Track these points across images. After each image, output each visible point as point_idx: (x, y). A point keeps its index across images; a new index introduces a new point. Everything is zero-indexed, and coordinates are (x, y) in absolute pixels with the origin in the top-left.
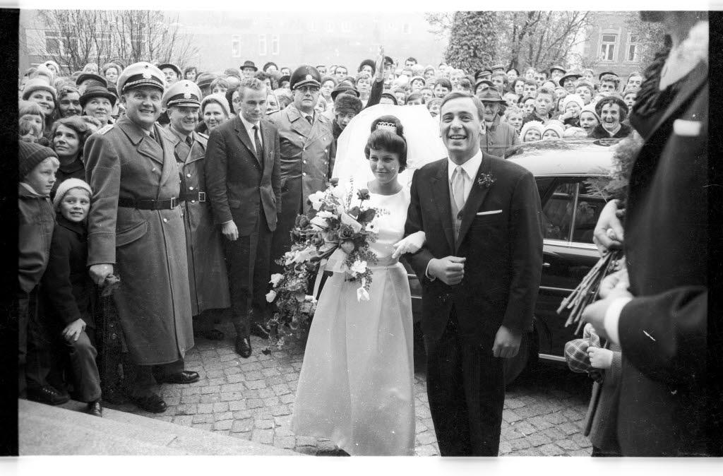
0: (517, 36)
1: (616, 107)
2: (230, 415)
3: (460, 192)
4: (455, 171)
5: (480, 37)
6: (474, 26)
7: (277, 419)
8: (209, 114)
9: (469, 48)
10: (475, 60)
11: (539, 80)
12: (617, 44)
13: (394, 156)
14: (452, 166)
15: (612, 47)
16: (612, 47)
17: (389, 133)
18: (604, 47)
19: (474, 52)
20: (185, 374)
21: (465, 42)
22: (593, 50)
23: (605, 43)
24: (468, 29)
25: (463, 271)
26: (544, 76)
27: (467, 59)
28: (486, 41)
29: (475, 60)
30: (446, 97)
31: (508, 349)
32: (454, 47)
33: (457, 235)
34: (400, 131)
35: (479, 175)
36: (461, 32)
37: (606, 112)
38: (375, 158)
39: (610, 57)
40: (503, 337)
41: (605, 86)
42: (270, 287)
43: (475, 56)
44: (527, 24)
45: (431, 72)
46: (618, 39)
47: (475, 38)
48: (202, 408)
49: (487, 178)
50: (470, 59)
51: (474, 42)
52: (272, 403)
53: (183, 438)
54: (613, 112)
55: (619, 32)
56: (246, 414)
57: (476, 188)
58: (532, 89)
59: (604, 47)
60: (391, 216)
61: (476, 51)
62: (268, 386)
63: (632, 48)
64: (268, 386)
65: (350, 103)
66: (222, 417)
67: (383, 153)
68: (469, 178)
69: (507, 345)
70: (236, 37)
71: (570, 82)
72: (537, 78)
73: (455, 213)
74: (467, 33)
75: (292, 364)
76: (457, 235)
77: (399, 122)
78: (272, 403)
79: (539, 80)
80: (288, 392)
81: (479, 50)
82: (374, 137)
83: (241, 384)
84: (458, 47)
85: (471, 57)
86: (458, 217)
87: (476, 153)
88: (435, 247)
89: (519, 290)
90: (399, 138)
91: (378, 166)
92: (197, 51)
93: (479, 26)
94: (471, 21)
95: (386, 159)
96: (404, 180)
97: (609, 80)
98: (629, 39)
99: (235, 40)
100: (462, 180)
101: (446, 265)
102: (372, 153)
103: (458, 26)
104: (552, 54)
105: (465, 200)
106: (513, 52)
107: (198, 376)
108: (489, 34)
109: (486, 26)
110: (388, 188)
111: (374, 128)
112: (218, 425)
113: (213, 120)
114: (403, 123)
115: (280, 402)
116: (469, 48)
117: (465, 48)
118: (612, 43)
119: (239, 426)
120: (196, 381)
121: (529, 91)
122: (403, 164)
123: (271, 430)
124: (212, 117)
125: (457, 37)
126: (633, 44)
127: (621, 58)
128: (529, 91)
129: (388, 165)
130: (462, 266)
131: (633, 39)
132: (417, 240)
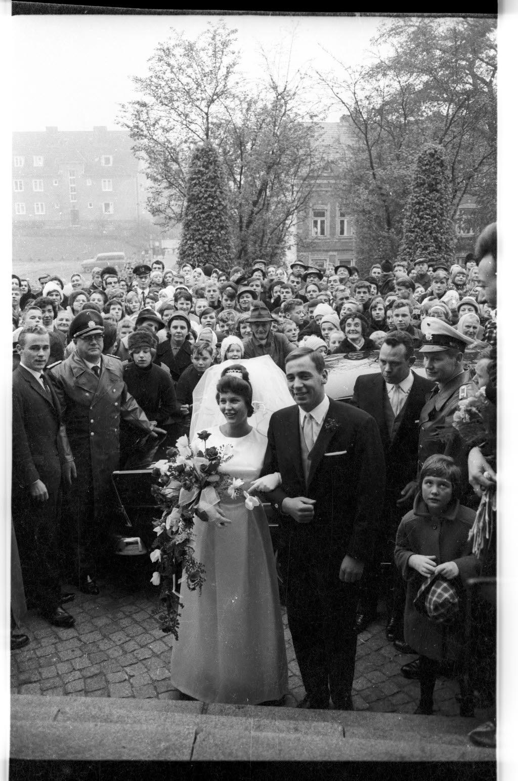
0: (244, 225)
2: (77, 674)
5: (214, 231)
6: (207, 221)
7: (128, 669)
9: (204, 243)
10: (210, 255)
11: (295, 284)
14: (302, 413)
15: (323, 222)
16: (323, 222)
18: (316, 222)
19: (209, 247)
23: (316, 219)
24: (201, 224)
26: (300, 280)
27: (202, 253)
28: (220, 235)
29: (210, 255)
33: (307, 474)
34: (246, 376)
35: (326, 421)
39: (322, 232)
40: (347, 564)
43: (210, 251)
45: (169, 275)
46: (328, 214)
47: (208, 232)
48: (46, 673)
50: (206, 255)
51: (209, 237)
52: (116, 653)
53: (67, 709)
55: (328, 207)
56: (94, 670)
58: (287, 292)
59: (316, 222)
60: (244, 456)
62: (105, 636)
63: (342, 222)
64: (105, 636)
65: (141, 338)
66: (71, 678)
71: (312, 279)
72: (293, 282)
73: (305, 456)
74: (201, 228)
75: (121, 609)
76: (307, 474)
77: (245, 369)
78: (116, 653)
79: (295, 284)
80: (128, 639)
83: (76, 639)
84: (192, 242)
85: (206, 251)
86: (308, 459)
88: (288, 488)
90: (245, 382)
93: (211, 221)
94: (203, 216)
98: (338, 214)
107: (27, 639)
108: (222, 228)
109: (218, 220)
110: (239, 429)
112: (69, 687)
115: (125, 652)
116: (204, 243)
117: (200, 242)
118: (323, 219)
119: (93, 684)
120: (27, 644)
123: (126, 682)
127: (333, 234)
128: (285, 294)
131: (342, 215)
132: (271, 481)
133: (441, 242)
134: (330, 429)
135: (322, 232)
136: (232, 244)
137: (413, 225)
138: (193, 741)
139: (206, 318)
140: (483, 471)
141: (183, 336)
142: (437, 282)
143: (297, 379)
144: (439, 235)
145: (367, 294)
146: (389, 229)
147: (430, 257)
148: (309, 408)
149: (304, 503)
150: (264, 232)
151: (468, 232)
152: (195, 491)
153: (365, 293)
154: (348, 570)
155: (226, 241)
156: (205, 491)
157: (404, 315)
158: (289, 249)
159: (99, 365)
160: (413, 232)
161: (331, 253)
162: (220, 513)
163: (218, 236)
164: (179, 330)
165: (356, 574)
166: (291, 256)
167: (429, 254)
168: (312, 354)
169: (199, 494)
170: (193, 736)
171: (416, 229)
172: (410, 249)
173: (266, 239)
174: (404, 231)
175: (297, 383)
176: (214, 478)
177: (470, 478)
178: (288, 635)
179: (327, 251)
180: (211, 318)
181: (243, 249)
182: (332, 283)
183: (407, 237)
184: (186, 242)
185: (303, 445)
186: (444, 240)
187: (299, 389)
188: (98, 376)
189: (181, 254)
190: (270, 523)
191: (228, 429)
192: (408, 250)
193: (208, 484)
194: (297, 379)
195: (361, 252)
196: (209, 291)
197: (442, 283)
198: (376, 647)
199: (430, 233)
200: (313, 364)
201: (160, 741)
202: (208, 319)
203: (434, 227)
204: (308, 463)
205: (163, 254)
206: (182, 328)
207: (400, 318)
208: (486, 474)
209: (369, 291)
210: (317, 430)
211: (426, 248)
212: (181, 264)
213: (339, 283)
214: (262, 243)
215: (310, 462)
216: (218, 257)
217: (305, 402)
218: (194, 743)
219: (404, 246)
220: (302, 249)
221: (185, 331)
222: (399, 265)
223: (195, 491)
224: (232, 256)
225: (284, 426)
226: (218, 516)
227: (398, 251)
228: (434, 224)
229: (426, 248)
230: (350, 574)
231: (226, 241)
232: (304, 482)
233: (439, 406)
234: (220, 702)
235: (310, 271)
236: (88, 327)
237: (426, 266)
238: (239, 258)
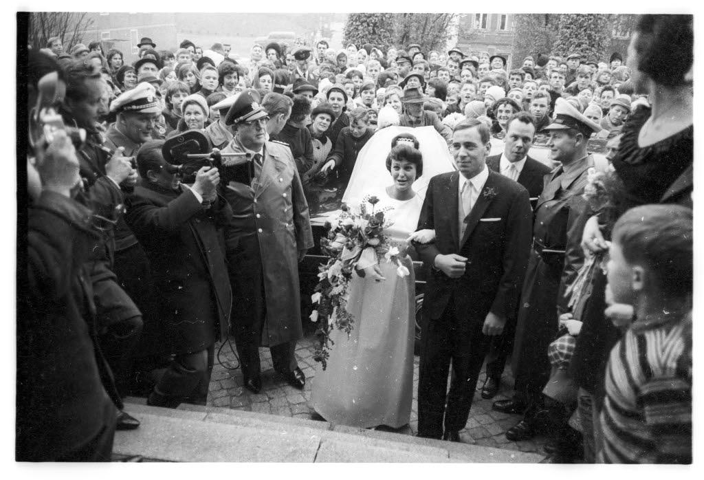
1: (509, 107)
3: (468, 199)
4: (465, 184)
8: (189, 113)
9: (368, 25)
11: (453, 68)
13: (413, 166)
14: (463, 180)
17: (409, 147)
19: (373, 29)
20: (237, 354)
21: (365, 19)
25: (465, 269)
30: (237, 65)
33: (462, 236)
34: (417, 146)
35: (484, 189)
37: (501, 111)
38: (397, 168)
39: (484, 26)
40: (490, 320)
41: (513, 79)
43: (374, 33)
49: (491, 191)
54: (507, 111)
57: (481, 199)
60: (404, 220)
61: (375, 29)
67: (404, 163)
68: (475, 190)
72: (451, 66)
73: (462, 218)
76: (462, 236)
81: (378, 27)
84: (358, 23)
85: (370, 34)
89: (506, 284)
91: (400, 174)
92: (93, 22)
95: (407, 168)
96: (420, 188)
97: (515, 74)
100: (469, 191)
101: (449, 261)
102: (394, 162)
104: (437, 27)
105: (472, 207)
106: (405, 26)
110: (404, 195)
111: (394, 144)
113: (193, 120)
114: (419, 140)
117: (365, 24)
121: (322, 49)
122: (419, 172)
124: (193, 117)
127: (493, 28)
129: (408, 173)
130: (464, 264)
133: (594, 40)
134: (488, 197)
135: (484, 26)
136: (394, 28)
137: (569, 22)
138: (317, 447)
139: (366, 93)
140: (594, 237)
141: (340, 107)
142: (581, 77)
143: (462, 148)
144: (593, 33)
145: (520, 82)
146: (546, 25)
147: (582, 54)
148: (469, 175)
149: (457, 260)
150: (427, 20)
151: (624, 35)
152: (357, 250)
153: (517, 80)
154: (492, 325)
155: (389, 24)
156: (366, 251)
157: (542, 106)
158: (450, 39)
159: (261, 152)
160: (569, 28)
161: (489, 47)
162: (376, 271)
163: (382, 19)
164: (336, 101)
165: (499, 329)
166: (451, 45)
167: (582, 51)
168: (480, 125)
169: (361, 252)
170: (318, 444)
171: (572, 26)
172: (564, 44)
173: (428, 27)
174: (560, 26)
175: (462, 151)
176: (375, 242)
177: (582, 244)
178: (416, 370)
179: (488, 45)
180: (371, 93)
181: (405, 34)
182: (482, 71)
183: (563, 33)
184: (352, 24)
185: (460, 209)
186: (597, 39)
187: (463, 158)
188: (261, 165)
189: (346, 35)
190: (417, 279)
191: (394, 191)
192: (562, 46)
193: (368, 246)
194: (462, 148)
195: (519, 46)
196: (371, 71)
197: (587, 77)
198: (149, 91)
199: (585, 30)
200: (479, 136)
201: (289, 445)
202: (369, 94)
203: (590, 25)
204: (463, 226)
205: (330, 37)
206: (339, 99)
207: (538, 108)
208: (595, 240)
209: (523, 79)
210: (476, 196)
211: (579, 45)
212: (346, 45)
213: (488, 70)
214: (424, 30)
215: (466, 225)
216: (381, 39)
217: (466, 169)
218: (318, 450)
219: (559, 42)
220: (463, 40)
221: (342, 103)
222: (553, 59)
223: (357, 250)
224: (394, 40)
225: (443, 190)
226: (375, 273)
227: (553, 46)
228: (590, 22)
229: (579, 45)
230: (493, 329)
231: (389, 24)
232: (458, 243)
233: (565, 185)
234: (346, 424)
235: (466, 59)
236: (252, 110)
237: (578, 62)
238: (401, 43)
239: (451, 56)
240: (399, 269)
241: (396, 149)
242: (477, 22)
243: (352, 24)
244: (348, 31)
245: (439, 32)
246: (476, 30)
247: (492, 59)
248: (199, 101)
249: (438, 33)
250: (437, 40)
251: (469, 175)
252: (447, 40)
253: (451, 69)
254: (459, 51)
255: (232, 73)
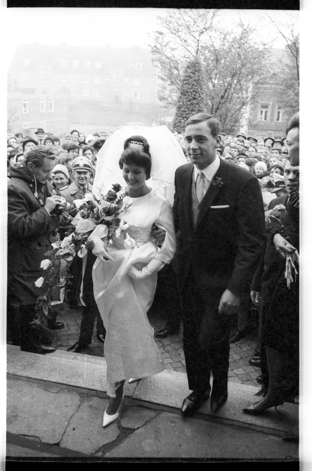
4: (198, 175)
12: (269, 110)
14: (197, 171)
15: (266, 112)
16: (266, 112)
18: (262, 112)
21: (185, 115)
22: (255, 117)
24: (187, 108)
31: (230, 307)
32: (179, 118)
34: (146, 149)
35: (215, 178)
36: (183, 109)
39: (265, 119)
42: (40, 272)
44: (220, 103)
46: (270, 107)
47: (191, 113)
55: (271, 103)
59: (262, 112)
67: (135, 167)
69: (229, 303)
70: (26, 100)
72: (239, 145)
77: (146, 141)
82: (126, 154)
87: (214, 159)
89: (243, 262)
94: (189, 103)
99: (25, 102)
102: (125, 166)
103: (181, 105)
104: (234, 120)
109: (197, 106)
111: (126, 146)
118: (266, 110)
124: (59, 181)
125: (181, 112)
126: (279, 110)
127: (272, 120)
131: (279, 108)
134: (216, 186)
148: (202, 167)
158: (242, 127)
173: (227, 120)
175: (193, 145)
184: (177, 118)
185: (194, 197)
187: (194, 150)
214: (224, 122)
220: (250, 128)
239: (239, 138)
240: (126, 240)
241: (129, 151)
242: (261, 116)
243: (177, 118)
244: (175, 123)
245: (235, 123)
246: (260, 121)
247: (265, 141)
248: (61, 170)
249: (233, 124)
250: (233, 128)
251: (202, 167)
252: (240, 128)
253: (238, 147)
254: (243, 135)
255: (75, 149)
